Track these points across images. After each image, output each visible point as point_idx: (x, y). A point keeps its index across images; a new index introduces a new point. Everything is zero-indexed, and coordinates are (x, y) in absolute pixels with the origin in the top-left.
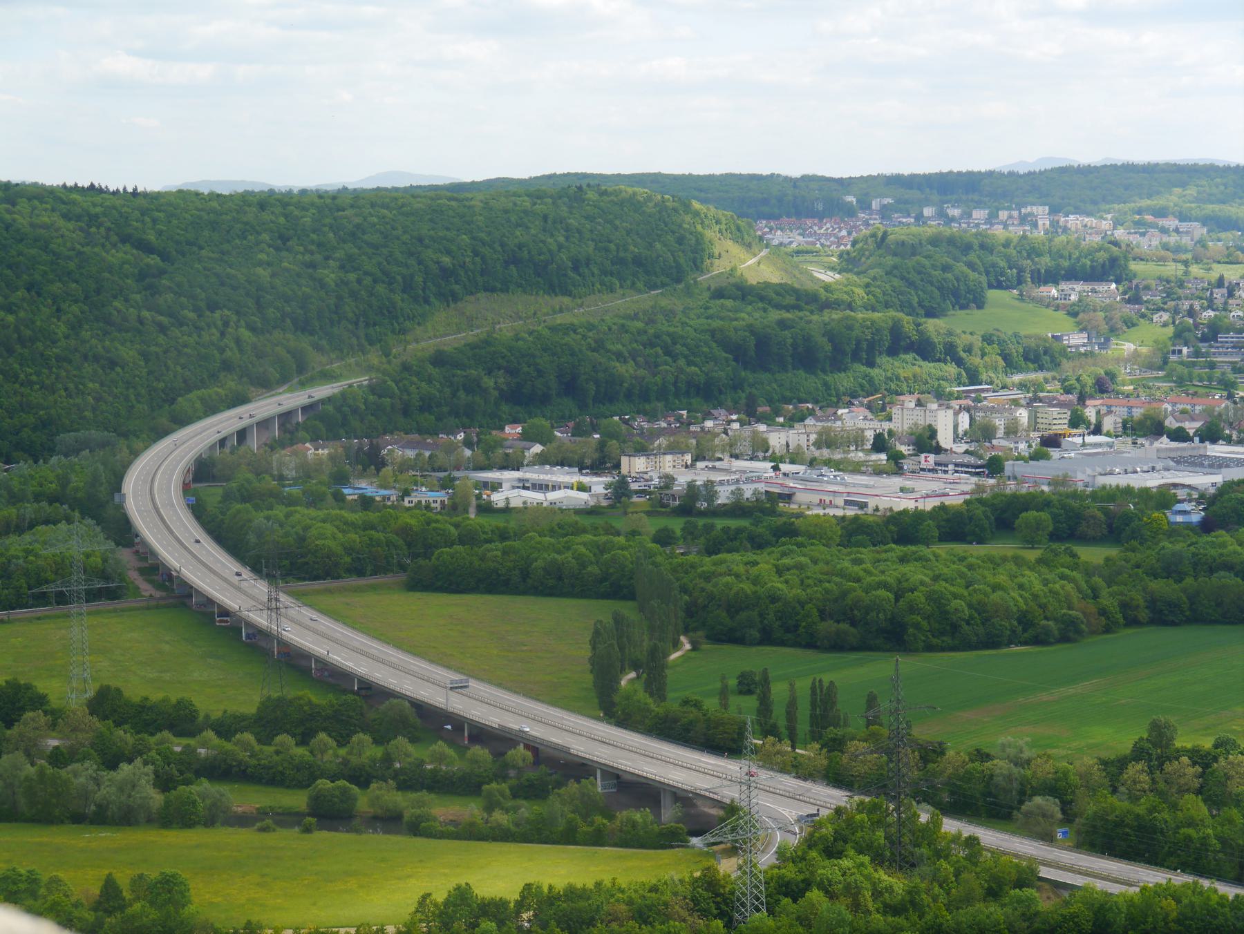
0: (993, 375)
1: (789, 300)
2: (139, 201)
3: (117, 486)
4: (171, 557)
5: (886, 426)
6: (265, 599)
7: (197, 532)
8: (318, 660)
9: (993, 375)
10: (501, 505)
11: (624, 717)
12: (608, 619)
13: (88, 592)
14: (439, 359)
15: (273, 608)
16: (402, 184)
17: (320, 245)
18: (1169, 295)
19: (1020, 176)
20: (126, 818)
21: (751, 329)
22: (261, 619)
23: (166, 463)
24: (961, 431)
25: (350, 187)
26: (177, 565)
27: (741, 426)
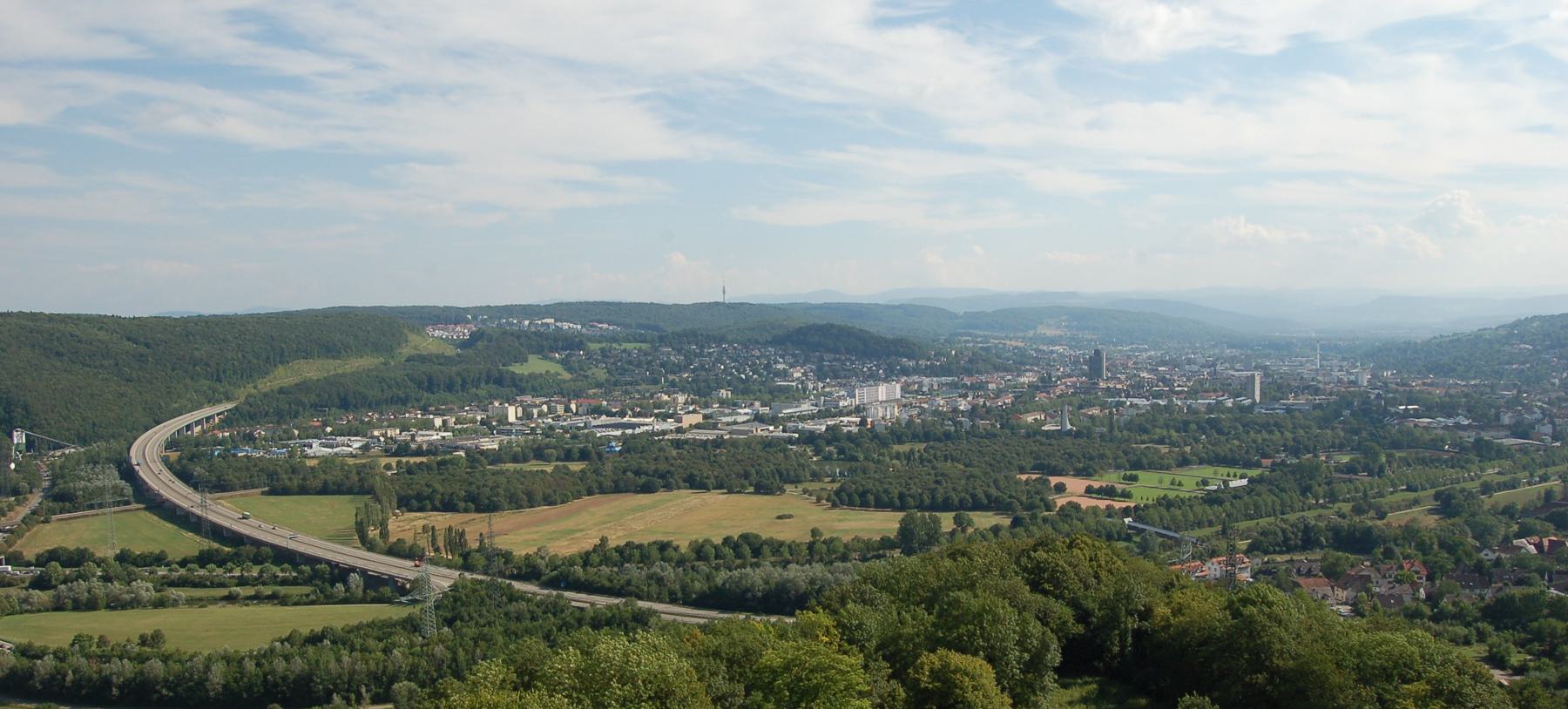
0: (1096, 611)
1: (442, 361)
2: (135, 322)
3: (129, 449)
4: (166, 493)
6: (199, 501)
7: (174, 478)
8: (227, 529)
9: (1096, 611)
11: (369, 546)
12: (361, 505)
14: (281, 391)
15: (203, 506)
16: (262, 311)
25: (239, 314)
26: (157, 488)
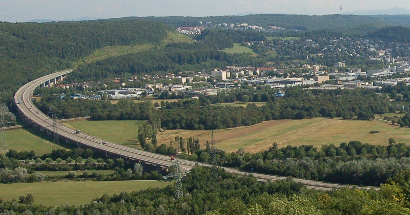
1: (186, 47)
4: (34, 119)
5: (317, 82)
7: (39, 111)
10: (115, 98)
11: (146, 148)
13: (5, 124)
14: (98, 63)
15: (55, 126)
17: (66, 36)
18: (275, 44)
19: (237, 16)
20: (17, 179)
21: (176, 53)
22: (52, 129)
23: (26, 91)
24: (228, 77)
25: (74, 21)
26: (29, 117)
27: (175, 77)
